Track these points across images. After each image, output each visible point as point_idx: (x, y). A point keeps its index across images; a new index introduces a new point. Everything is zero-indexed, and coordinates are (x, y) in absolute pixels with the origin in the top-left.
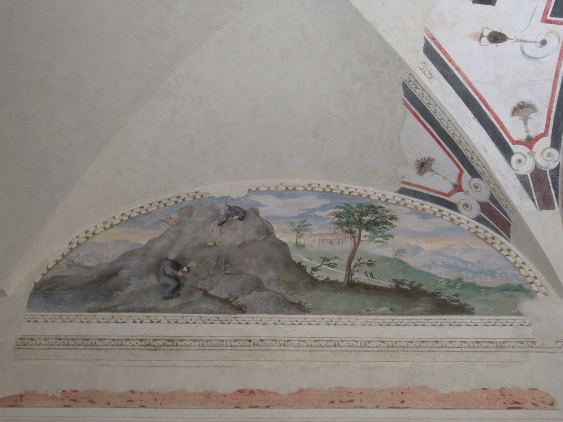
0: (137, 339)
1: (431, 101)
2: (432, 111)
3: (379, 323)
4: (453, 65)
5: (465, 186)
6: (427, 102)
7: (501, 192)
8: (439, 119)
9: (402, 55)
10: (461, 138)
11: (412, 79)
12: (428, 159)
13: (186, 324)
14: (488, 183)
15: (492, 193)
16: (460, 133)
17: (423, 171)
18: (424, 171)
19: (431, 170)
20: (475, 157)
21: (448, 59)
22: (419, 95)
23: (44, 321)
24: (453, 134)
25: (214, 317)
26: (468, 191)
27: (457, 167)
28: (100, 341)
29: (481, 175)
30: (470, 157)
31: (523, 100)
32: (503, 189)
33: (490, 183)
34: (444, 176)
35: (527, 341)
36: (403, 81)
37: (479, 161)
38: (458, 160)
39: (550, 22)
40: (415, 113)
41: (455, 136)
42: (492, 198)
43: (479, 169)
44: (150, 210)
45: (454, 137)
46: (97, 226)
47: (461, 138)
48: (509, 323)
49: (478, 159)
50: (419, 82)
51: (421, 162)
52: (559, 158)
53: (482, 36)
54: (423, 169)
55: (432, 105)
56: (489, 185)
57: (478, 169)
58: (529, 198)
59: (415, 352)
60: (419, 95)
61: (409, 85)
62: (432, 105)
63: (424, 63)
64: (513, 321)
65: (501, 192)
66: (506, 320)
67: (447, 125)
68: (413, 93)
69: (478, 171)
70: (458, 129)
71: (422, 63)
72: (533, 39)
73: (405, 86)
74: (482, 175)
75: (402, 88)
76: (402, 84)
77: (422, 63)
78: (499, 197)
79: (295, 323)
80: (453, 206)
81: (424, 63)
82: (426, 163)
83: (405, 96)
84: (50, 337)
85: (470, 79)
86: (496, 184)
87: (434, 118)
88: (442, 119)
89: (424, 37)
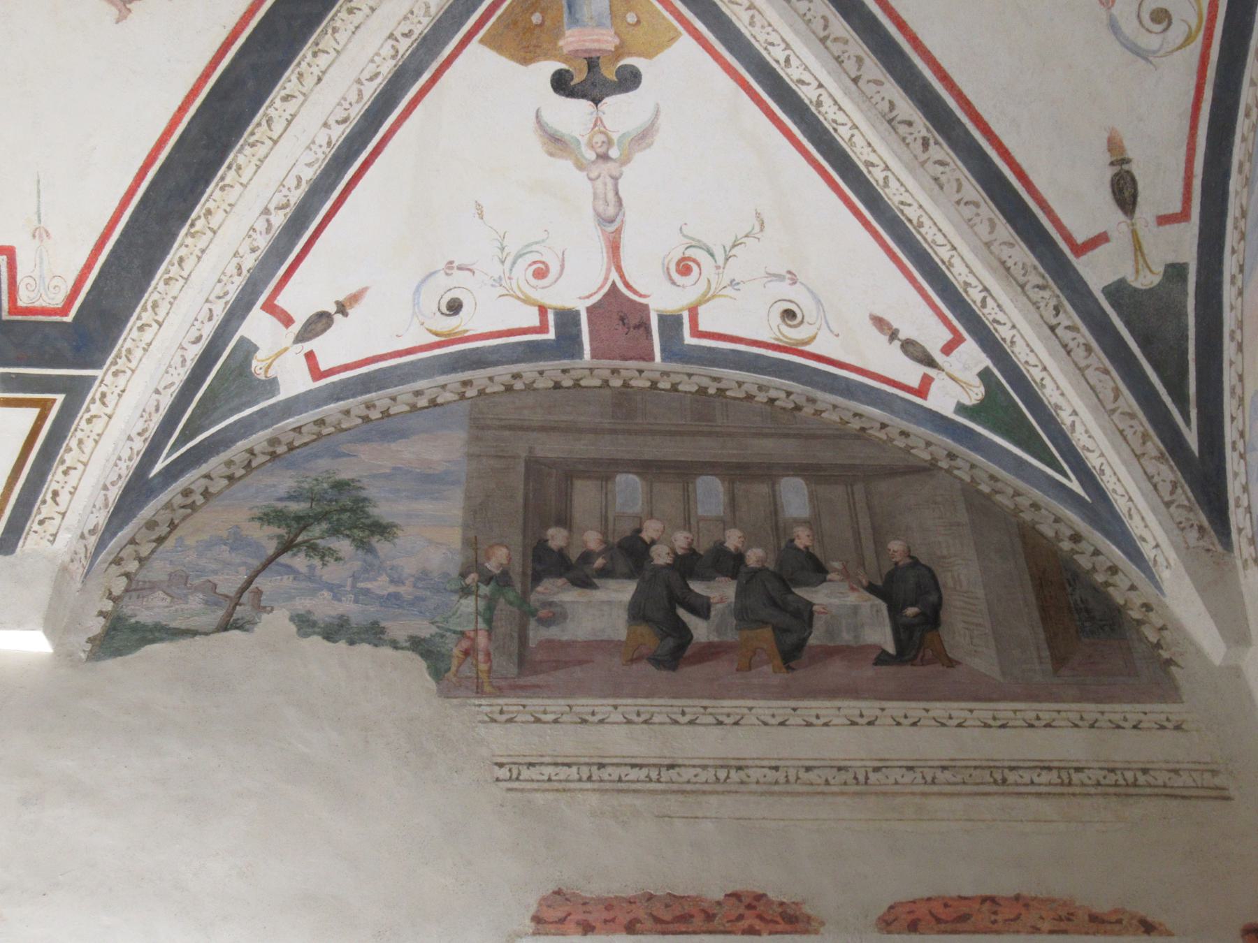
3: (939, 720)
13: (534, 726)
23: (715, 722)
28: (671, 771)
33: (1030, 365)
48: (1041, 721)
78: (1053, 401)
79: (814, 720)
84: (750, 763)
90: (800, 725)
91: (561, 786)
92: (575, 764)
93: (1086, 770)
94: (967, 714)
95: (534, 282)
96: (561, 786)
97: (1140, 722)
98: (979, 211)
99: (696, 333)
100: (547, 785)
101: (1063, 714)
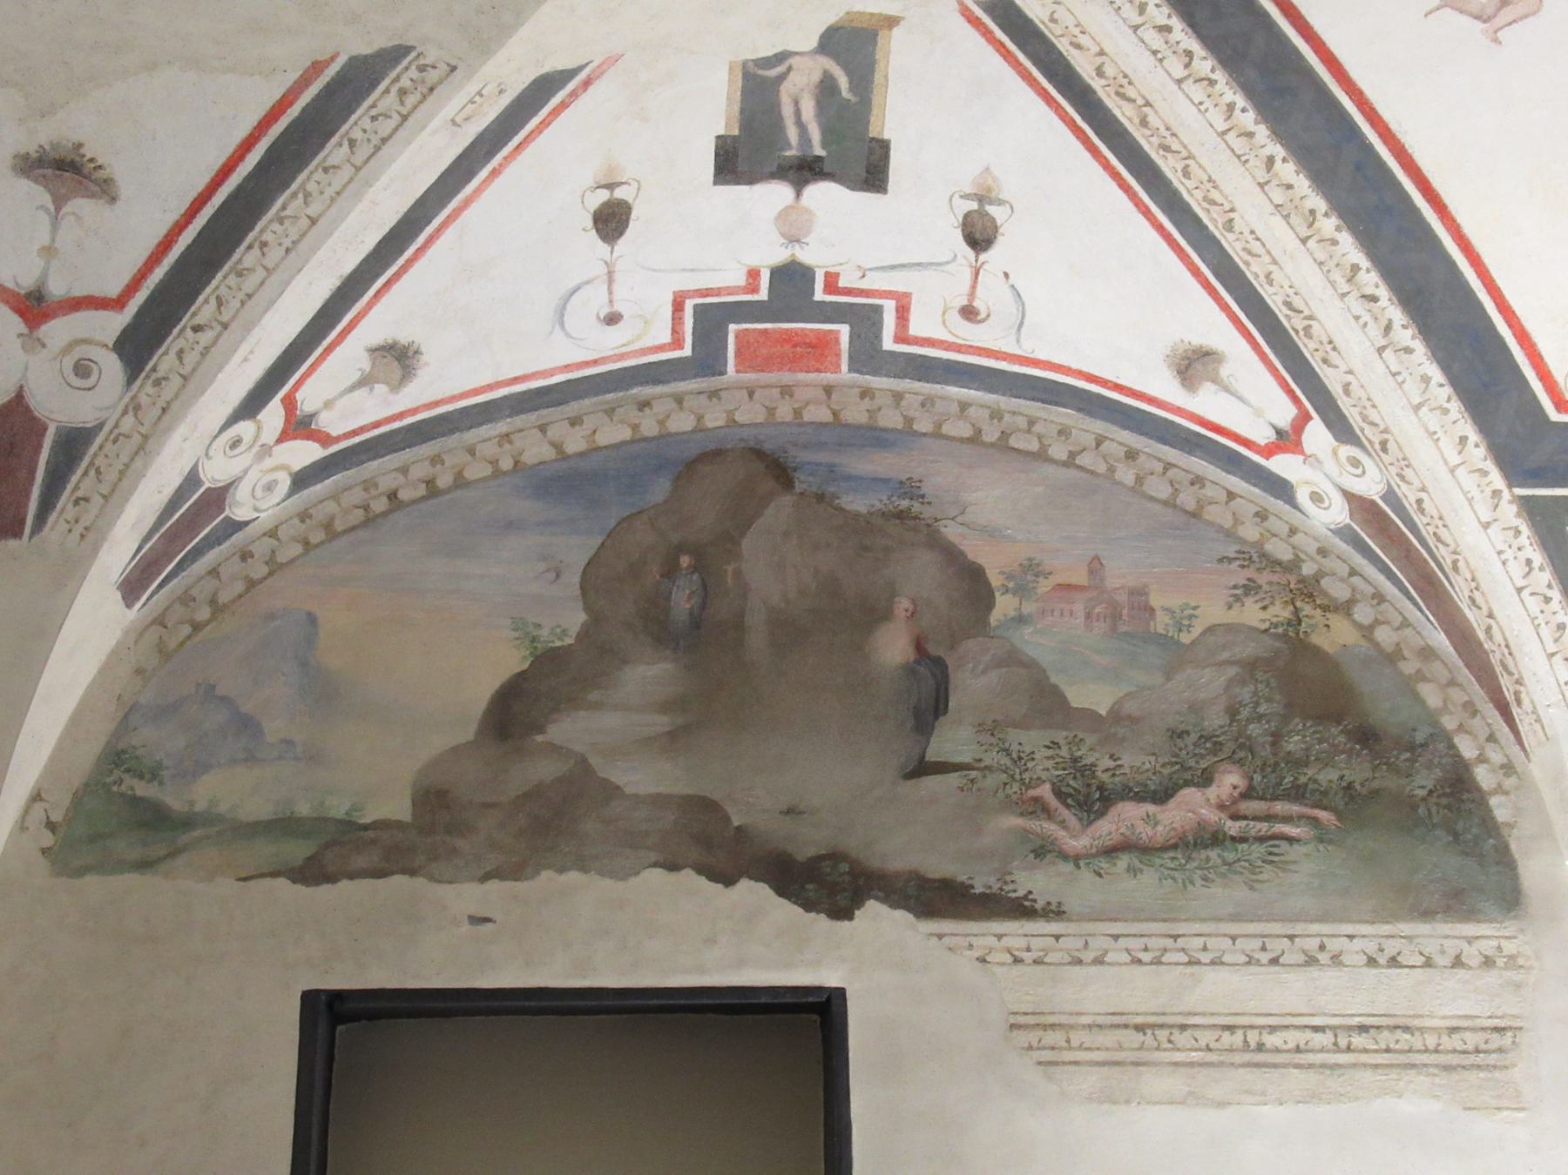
1: (362, 152)
2: (328, 155)
4: (505, 158)
5: (58, 330)
6: (357, 134)
7: (127, 466)
8: (303, 185)
9: (525, 32)
10: (261, 273)
11: (432, 76)
12: (108, 182)
14: (131, 409)
15: (96, 435)
16: (277, 265)
17: (40, 171)
18: (44, 176)
19: (59, 202)
20: (206, 337)
21: (525, 139)
22: (373, 106)
24: (264, 244)
26: (44, 346)
27: (126, 282)
29: (143, 375)
30: (198, 320)
31: (423, 349)
32: (146, 467)
34: (56, 245)
36: (415, 48)
37: (202, 354)
38: (157, 281)
39: (678, 306)
40: (291, 104)
41: (256, 251)
42: (74, 443)
43: (164, 360)
45: (250, 247)
47: (261, 273)
49: (207, 349)
50: (431, 99)
51: (78, 159)
52: (266, 510)
53: (610, 186)
54: (49, 172)
55: (353, 153)
56: (125, 413)
57: (165, 357)
58: (141, 538)
60: (373, 106)
61: (407, 69)
62: (353, 153)
63: (501, 92)
65: (127, 466)
67: (290, 217)
68: (373, 85)
69: (155, 358)
70: (293, 254)
71: (502, 86)
72: (617, 295)
73: (394, 55)
74: (148, 377)
75: (383, 46)
76: (400, 45)
77: (502, 86)
81: (501, 92)
82: (85, 177)
83: (352, 59)
85: (467, 213)
86: (146, 437)
87: (300, 170)
88: (307, 195)
89: (592, 62)
91: (1402, 1059)
92: (1510, 1028)
93: (1372, 1031)
94: (992, 941)
96: (1402, 1059)
97: (1106, 952)
98: (1435, 530)
99: (677, 343)
101: (1122, 942)
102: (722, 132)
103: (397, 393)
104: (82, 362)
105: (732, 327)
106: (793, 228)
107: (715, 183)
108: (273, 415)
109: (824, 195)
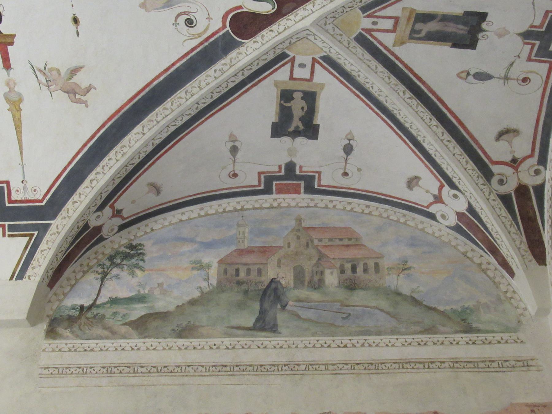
0: (391, 363)
25: (234, 341)
35: (449, 362)
44: (408, 223)
46: (89, 258)
59: (333, 375)
64: (380, 341)
66: (438, 338)
80: (432, 216)
90: (336, 347)
95: (20, 191)
99: (259, 185)
100: (170, 374)
102: (274, 121)
103: (420, 177)
104: (528, 79)
105: (274, 183)
106: (291, 152)
107: (271, 137)
108: (108, 211)
109: (300, 140)
